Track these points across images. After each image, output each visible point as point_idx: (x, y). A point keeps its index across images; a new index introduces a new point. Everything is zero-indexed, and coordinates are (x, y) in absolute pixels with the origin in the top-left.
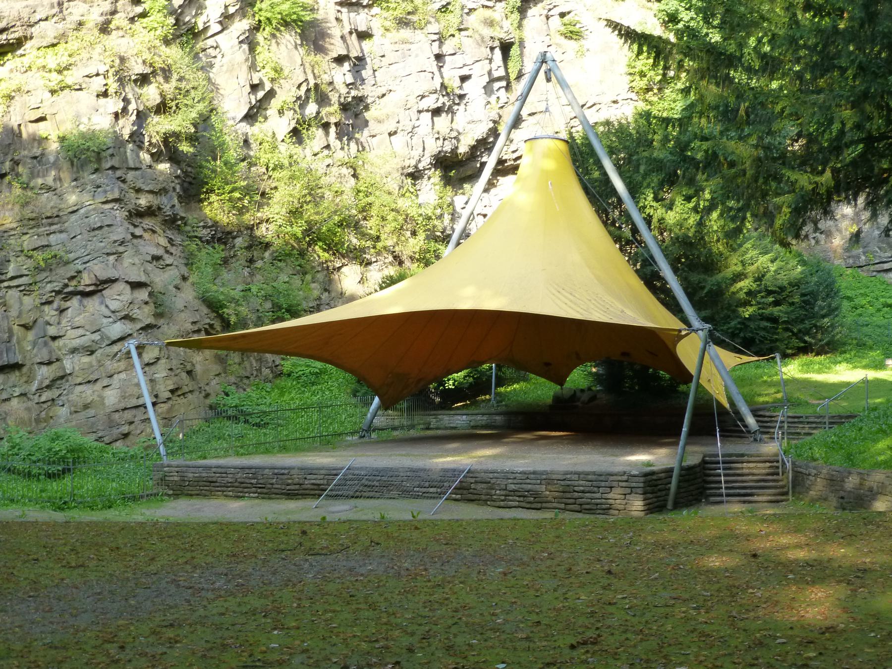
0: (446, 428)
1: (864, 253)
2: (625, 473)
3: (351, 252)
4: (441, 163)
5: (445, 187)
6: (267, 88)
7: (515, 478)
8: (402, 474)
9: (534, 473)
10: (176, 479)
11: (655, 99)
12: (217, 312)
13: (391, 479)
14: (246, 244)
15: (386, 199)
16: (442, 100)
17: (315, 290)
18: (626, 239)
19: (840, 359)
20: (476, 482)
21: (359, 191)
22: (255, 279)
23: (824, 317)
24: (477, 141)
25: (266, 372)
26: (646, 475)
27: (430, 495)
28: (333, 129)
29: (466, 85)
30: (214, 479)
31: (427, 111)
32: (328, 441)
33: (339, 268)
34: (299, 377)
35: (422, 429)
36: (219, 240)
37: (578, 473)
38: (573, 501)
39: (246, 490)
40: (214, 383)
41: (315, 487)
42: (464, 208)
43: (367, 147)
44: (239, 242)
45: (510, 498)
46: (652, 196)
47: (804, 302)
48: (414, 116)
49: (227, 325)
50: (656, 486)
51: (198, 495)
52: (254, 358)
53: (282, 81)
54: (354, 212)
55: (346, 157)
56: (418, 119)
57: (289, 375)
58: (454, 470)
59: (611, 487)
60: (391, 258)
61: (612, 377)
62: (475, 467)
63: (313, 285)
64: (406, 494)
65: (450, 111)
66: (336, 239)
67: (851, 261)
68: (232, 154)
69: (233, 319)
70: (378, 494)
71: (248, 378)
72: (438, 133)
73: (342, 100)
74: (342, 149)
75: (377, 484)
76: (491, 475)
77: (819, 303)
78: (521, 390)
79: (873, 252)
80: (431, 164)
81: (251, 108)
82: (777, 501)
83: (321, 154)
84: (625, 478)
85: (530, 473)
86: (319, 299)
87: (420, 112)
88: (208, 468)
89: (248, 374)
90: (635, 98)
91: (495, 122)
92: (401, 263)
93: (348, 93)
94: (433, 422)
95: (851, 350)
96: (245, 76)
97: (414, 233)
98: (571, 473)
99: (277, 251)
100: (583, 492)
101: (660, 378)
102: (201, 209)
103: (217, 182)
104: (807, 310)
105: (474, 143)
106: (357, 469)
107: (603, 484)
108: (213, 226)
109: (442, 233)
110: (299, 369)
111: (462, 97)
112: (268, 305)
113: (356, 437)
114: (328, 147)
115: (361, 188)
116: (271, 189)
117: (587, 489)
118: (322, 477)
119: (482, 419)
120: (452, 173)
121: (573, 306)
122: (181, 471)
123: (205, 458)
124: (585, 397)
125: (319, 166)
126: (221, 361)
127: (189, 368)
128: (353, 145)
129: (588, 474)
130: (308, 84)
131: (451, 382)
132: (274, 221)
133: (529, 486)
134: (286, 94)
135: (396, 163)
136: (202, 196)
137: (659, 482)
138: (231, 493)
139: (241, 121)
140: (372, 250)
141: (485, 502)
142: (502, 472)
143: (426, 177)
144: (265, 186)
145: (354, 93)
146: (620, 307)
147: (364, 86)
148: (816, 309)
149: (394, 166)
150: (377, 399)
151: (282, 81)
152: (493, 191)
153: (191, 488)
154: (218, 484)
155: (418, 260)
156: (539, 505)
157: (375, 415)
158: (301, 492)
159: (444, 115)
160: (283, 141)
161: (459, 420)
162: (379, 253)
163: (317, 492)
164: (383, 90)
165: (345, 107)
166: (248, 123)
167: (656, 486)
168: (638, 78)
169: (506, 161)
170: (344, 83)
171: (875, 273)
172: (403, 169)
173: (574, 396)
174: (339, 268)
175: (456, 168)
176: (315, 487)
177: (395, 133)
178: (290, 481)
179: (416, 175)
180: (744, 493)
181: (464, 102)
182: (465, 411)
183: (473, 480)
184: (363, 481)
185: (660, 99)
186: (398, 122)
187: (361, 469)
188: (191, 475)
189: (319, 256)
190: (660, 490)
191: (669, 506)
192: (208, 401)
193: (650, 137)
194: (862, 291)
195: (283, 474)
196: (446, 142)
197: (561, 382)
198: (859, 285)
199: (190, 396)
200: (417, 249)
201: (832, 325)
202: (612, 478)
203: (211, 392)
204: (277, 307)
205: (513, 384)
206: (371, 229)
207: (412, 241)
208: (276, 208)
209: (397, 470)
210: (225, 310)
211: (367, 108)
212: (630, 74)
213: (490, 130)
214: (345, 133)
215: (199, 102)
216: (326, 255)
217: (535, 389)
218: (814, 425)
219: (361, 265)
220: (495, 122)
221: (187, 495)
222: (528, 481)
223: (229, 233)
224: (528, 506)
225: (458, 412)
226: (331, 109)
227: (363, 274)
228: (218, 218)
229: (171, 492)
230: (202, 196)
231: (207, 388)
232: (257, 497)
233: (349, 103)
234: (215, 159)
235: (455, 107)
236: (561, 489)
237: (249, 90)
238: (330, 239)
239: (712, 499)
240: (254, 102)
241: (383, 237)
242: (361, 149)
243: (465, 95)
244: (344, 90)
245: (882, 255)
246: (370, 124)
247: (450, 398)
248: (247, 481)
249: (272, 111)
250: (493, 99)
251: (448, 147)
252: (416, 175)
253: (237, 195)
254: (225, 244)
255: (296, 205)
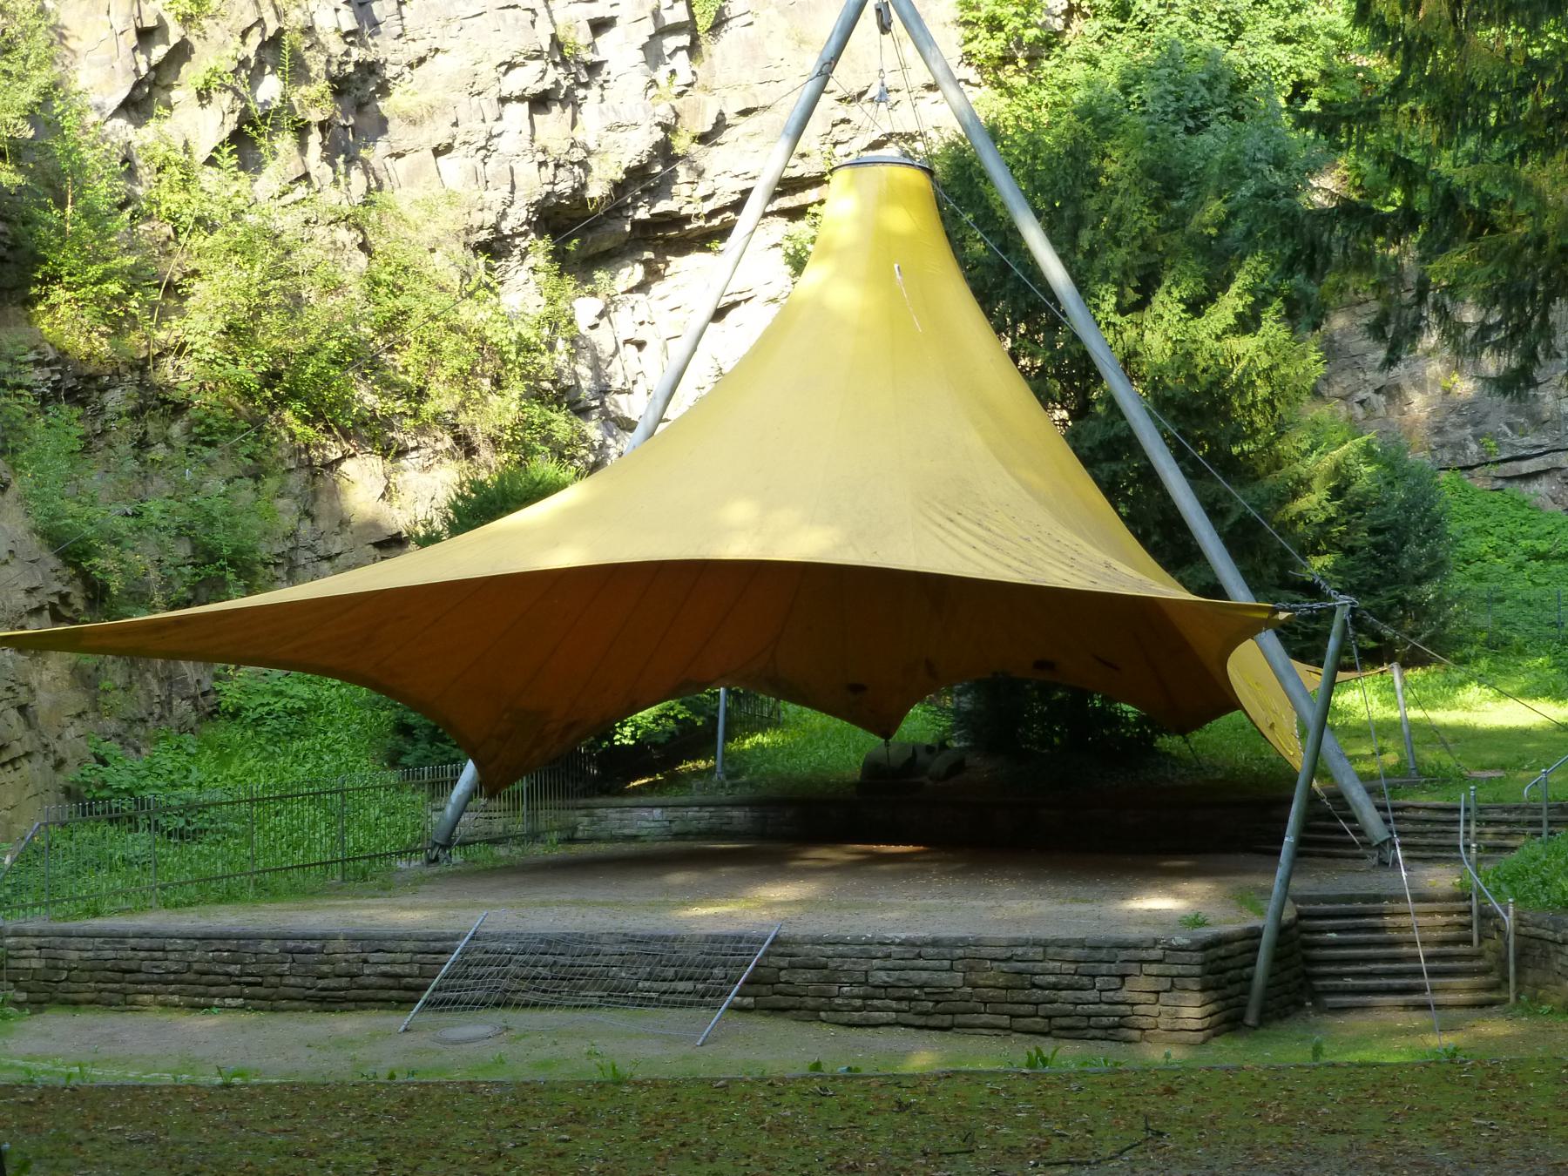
0: (614, 839)
1: (1476, 437)
2: (1156, 942)
3: (364, 424)
4: (547, 220)
5: (560, 276)
6: (174, 39)
7: (889, 956)
8: (607, 949)
9: (935, 943)
10: (35, 964)
11: (1020, 81)
12: (76, 566)
13: (579, 961)
14: (131, 405)
15: (439, 301)
16: (554, 74)
17: (286, 514)
18: (1065, 378)
19: (1458, 676)
20: (792, 966)
21: (378, 284)
22: (151, 489)
23: (1419, 580)
24: (628, 171)
25: (182, 707)
26: (1206, 946)
27: (681, 998)
28: (315, 138)
29: (604, 40)
30: (133, 965)
31: (520, 99)
32: (359, 871)
33: (338, 462)
34: (259, 721)
35: (560, 841)
36: (70, 393)
37: (1044, 944)
38: (1030, 1008)
39: (214, 990)
40: (70, 733)
41: (390, 982)
42: (595, 327)
43: (386, 181)
44: (116, 400)
45: (876, 1002)
46: (1114, 300)
47: (1375, 546)
48: (491, 110)
49: (97, 594)
50: (1223, 971)
51: (91, 1002)
52: (156, 675)
53: (205, 22)
54: (366, 331)
55: (345, 202)
56: (499, 118)
57: (235, 715)
58: (738, 939)
59: (1123, 977)
60: (448, 441)
61: (999, 714)
62: (786, 931)
63: (281, 503)
64: (618, 995)
65: (571, 101)
66: (330, 396)
67: (1446, 455)
68: (102, 191)
69: (116, 584)
70: (547, 998)
71: (143, 720)
72: (544, 151)
73: (334, 69)
74: (336, 182)
75: (545, 972)
76: (829, 950)
77: (1411, 548)
78: (776, 749)
79: (1495, 436)
80: (528, 222)
81: (138, 85)
82: (1491, 1003)
83: (287, 191)
84: (1156, 953)
85: (926, 944)
86: (293, 535)
87: (503, 101)
88: (119, 937)
89: (144, 714)
90: (976, 79)
91: (666, 128)
92: (470, 451)
93: (347, 53)
94: (583, 823)
95: (1477, 657)
96: (127, 10)
97: (497, 383)
98: (1025, 943)
99: (201, 422)
100: (1055, 987)
101: (1116, 720)
102: (29, 319)
103: (68, 259)
104: (1381, 566)
105: (620, 176)
106: (495, 937)
107: (1104, 968)
108: (57, 361)
109: (554, 382)
110: (258, 700)
111: (593, 68)
112: (183, 550)
113: (417, 862)
114: (306, 176)
115: (383, 276)
116: (186, 275)
117: (1066, 980)
118: (407, 957)
119: (695, 817)
120: (572, 246)
121: (992, 552)
122: (49, 944)
123: (97, 914)
124: (939, 764)
125: (288, 222)
126: (85, 680)
127: (23, 698)
128: (356, 175)
129: (1066, 944)
130: (264, 30)
131: (628, 731)
132: (194, 342)
133: (925, 975)
134: (216, 52)
135: (449, 220)
136: (34, 291)
137: (1230, 963)
138: (176, 998)
139: (115, 114)
140: (409, 422)
141: (812, 1014)
142: (856, 941)
143: (516, 252)
144: (172, 269)
145: (357, 54)
146: (1100, 556)
147: (377, 39)
148: (1405, 563)
149: (450, 226)
150: (469, 770)
151: (205, 22)
152: (657, 288)
153: (74, 986)
154: (142, 977)
155: (508, 446)
156: (948, 1020)
157: (463, 809)
158: (353, 993)
159: (556, 109)
160: (211, 161)
161: (642, 818)
162: (422, 430)
163: (393, 993)
164: (420, 49)
165: (341, 87)
166: (131, 120)
167: (1223, 971)
168: (983, 33)
169: (687, 219)
170: (337, 30)
171: (1499, 483)
172: (468, 232)
173: (913, 762)
174: (338, 462)
175: (594, 232)
176: (390, 982)
177: (449, 148)
178: (326, 968)
179: (495, 247)
180: (1403, 983)
181: (600, 79)
182: (656, 799)
183: (784, 962)
184: (512, 967)
185: (1031, 81)
186: (455, 124)
187: (506, 937)
188: (74, 955)
189: (292, 435)
190: (1231, 982)
191: (1251, 1019)
192: (61, 779)
193: (1094, 163)
194: (1477, 524)
195: (309, 951)
196: (562, 173)
197: (887, 735)
198: (1467, 508)
199: (25, 766)
200: (508, 420)
201: (1438, 599)
202: (1123, 955)
203: (68, 755)
204: (206, 555)
205: (752, 733)
206: (406, 372)
207: (494, 400)
208: (198, 321)
209: (594, 939)
210: (96, 560)
211: (384, 89)
212: (966, 23)
213: (656, 146)
214: (344, 146)
215: (39, 66)
216: (310, 431)
217: (806, 741)
218: (1504, 829)
219: (385, 457)
220: (666, 128)
221: (65, 1003)
222: (921, 963)
223: (92, 378)
224: (921, 1021)
225: (642, 800)
226: (312, 91)
227: (388, 478)
228: (68, 341)
229: (23, 996)
230: (34, 291)
231: (58, 746)
232: (242, 1007)
233: (347, 78)
234: (61, 204)
235: (581, 93)
236: (1001, 981)
237: (132, 39)
238: (311, 397)
239: (1331, 1000)
240: (144, 70)
241: (434, 388)
242: (374, 184)
243: (600, 64)
244: (337, 47)
245: (1517, 441)
246: (391, 126)
247: (616, 771)
248: (218, 969)
249: (183, 94)
250: (662, 74)
251: (565, 186)
252: (495, 247)
253: (114, 288)
254: (83, 403)
255: (243, 314)
